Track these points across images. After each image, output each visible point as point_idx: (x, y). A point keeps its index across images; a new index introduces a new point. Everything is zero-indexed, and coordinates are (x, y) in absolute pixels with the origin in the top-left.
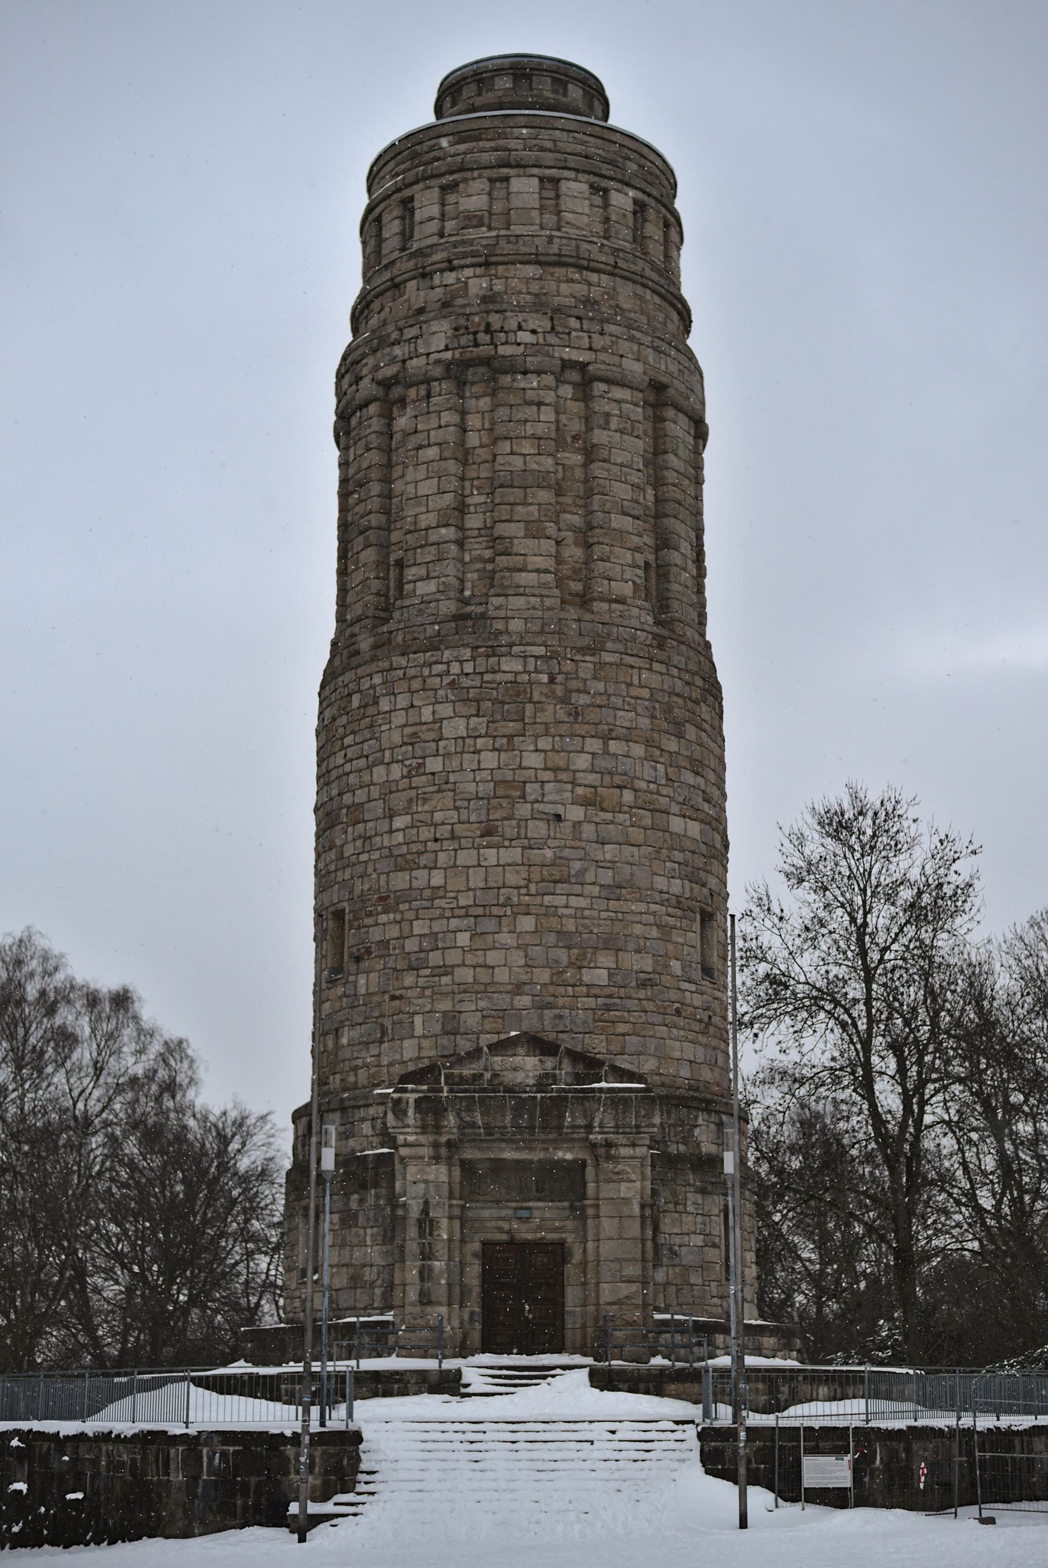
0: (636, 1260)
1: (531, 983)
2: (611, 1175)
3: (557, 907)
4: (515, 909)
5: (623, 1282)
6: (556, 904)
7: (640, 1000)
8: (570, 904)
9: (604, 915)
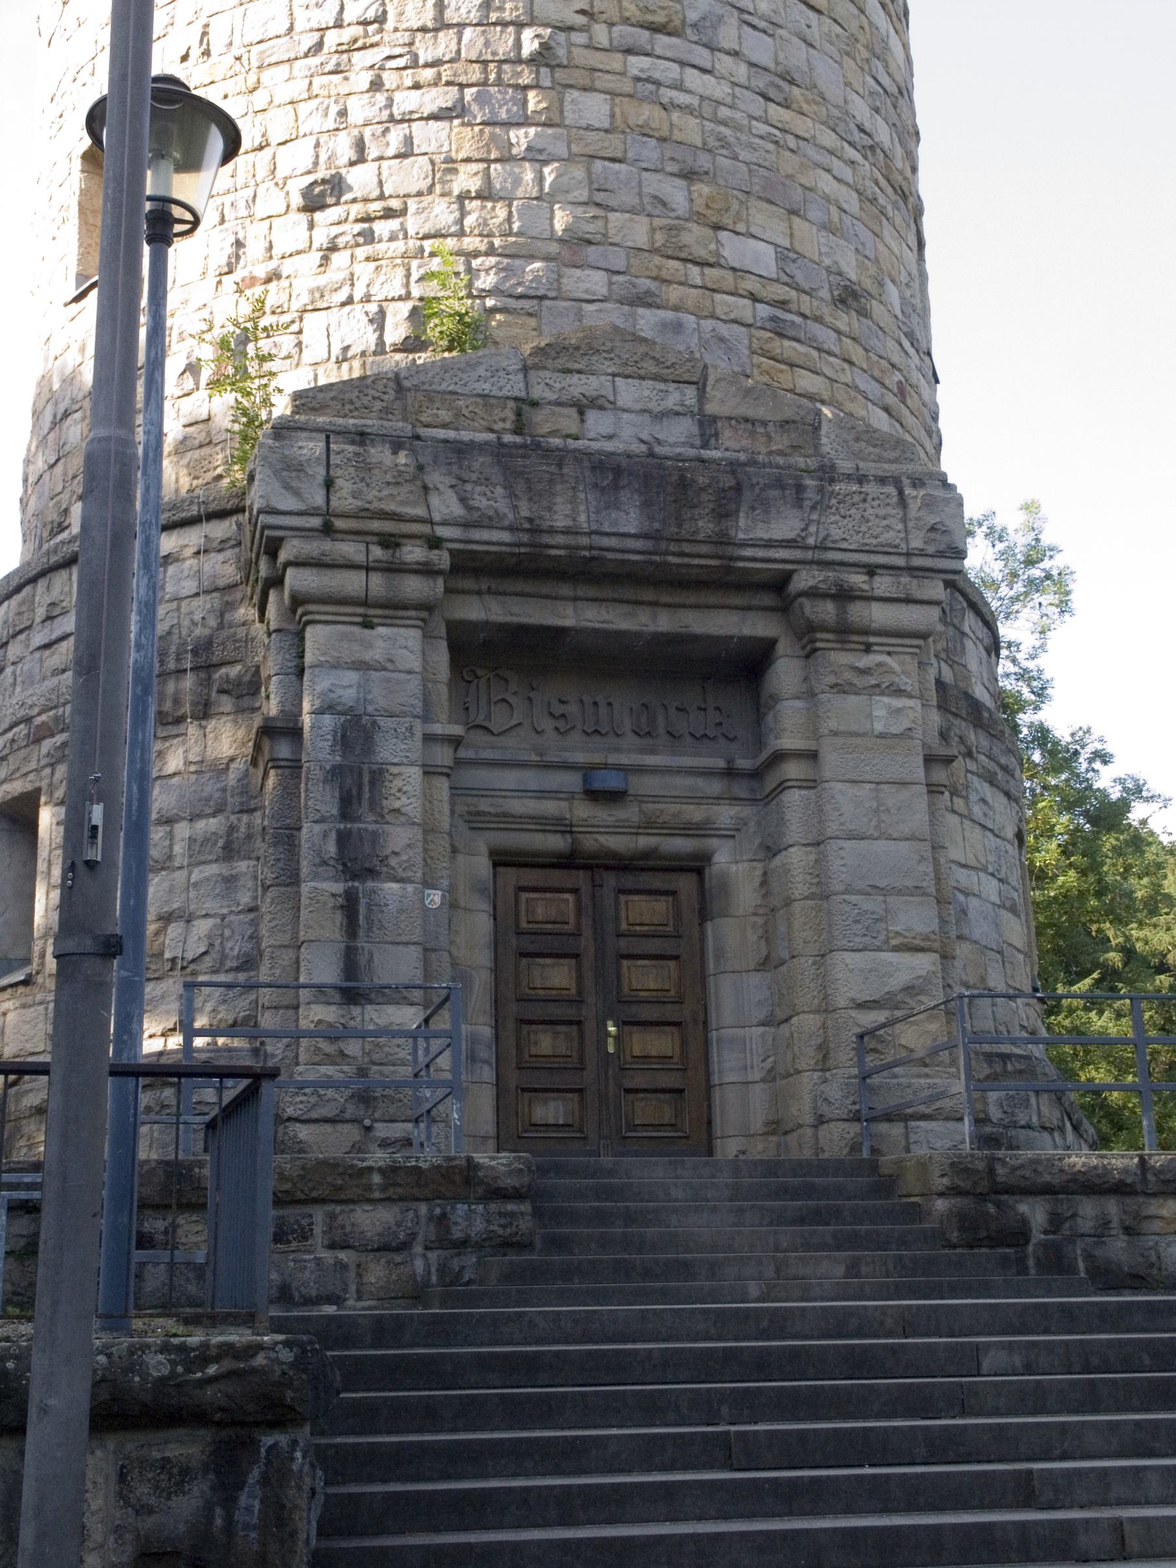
0: (918, 890)
1: (604, 240)
2: (848, 675)
3: (658, 83)
4: (560, 74)
5: (896, 949)
6: (657, 75)
7: (838, 332)
8: (688, 84)
9: (763, 129)
